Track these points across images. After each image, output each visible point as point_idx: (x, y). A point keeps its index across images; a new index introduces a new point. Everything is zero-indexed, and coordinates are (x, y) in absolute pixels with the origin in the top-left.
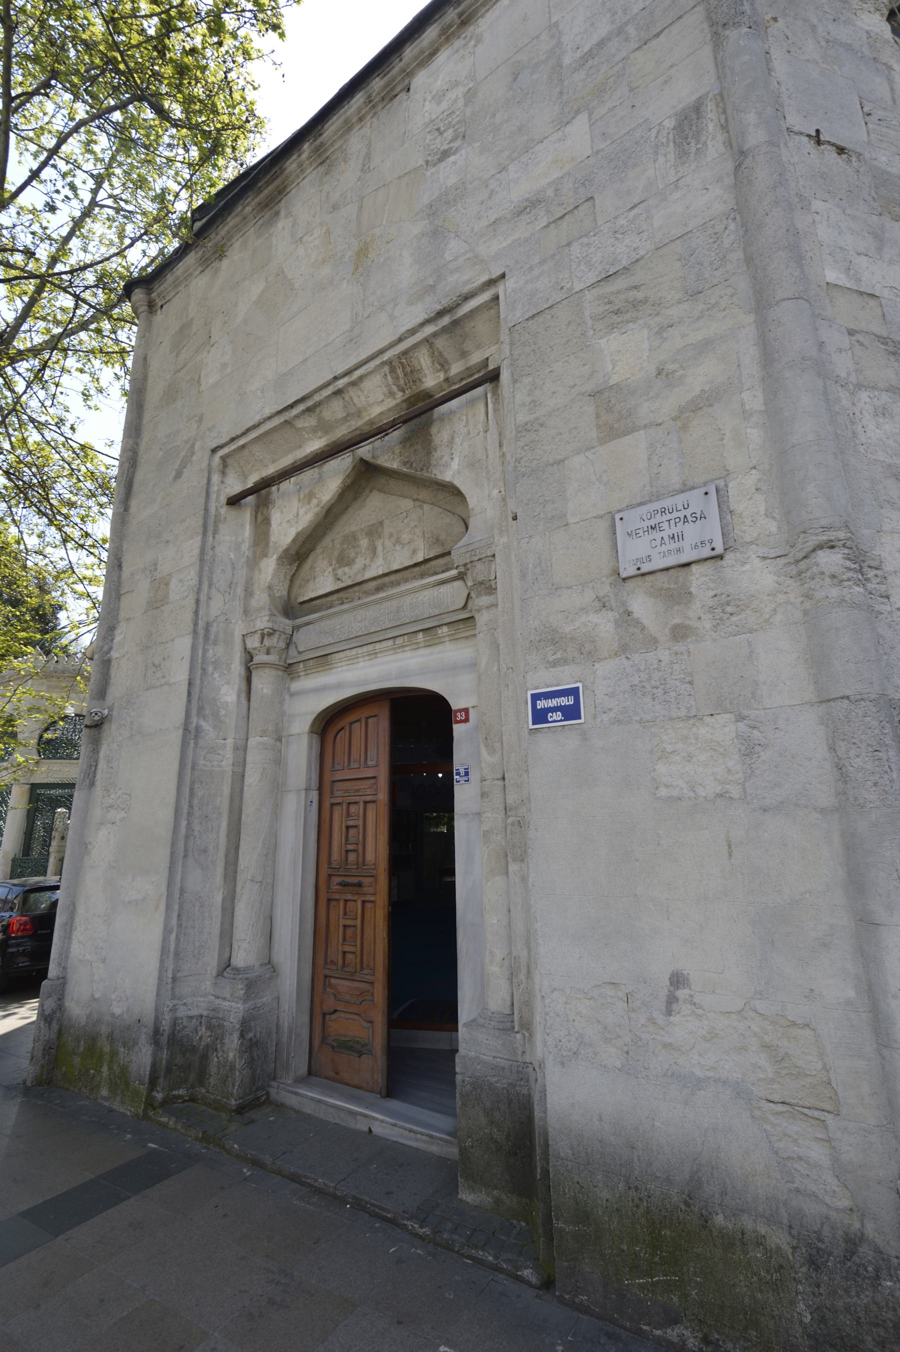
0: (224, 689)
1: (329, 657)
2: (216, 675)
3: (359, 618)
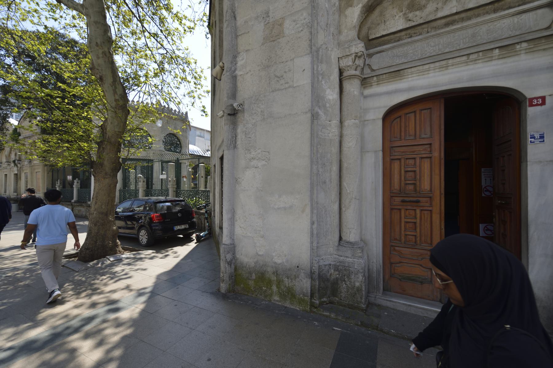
0: (328, 91)
1: (402, 71)
2: (323, 82)
3: (432, 44)
